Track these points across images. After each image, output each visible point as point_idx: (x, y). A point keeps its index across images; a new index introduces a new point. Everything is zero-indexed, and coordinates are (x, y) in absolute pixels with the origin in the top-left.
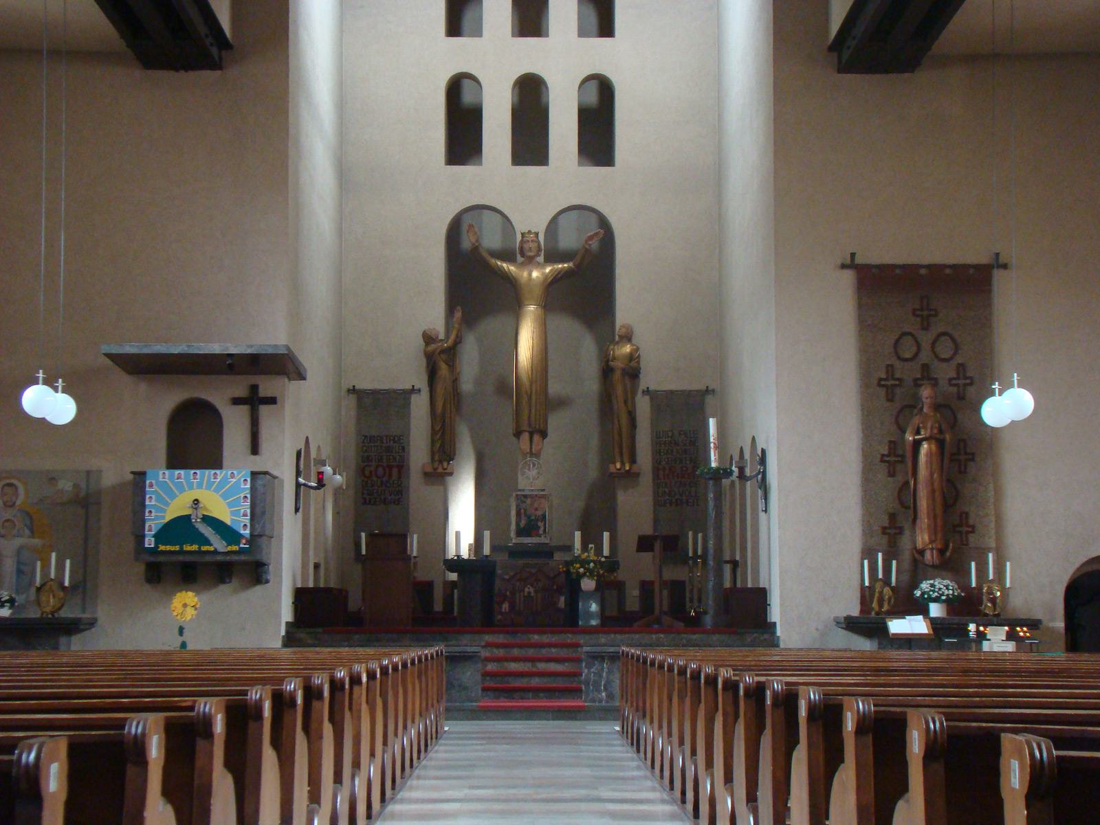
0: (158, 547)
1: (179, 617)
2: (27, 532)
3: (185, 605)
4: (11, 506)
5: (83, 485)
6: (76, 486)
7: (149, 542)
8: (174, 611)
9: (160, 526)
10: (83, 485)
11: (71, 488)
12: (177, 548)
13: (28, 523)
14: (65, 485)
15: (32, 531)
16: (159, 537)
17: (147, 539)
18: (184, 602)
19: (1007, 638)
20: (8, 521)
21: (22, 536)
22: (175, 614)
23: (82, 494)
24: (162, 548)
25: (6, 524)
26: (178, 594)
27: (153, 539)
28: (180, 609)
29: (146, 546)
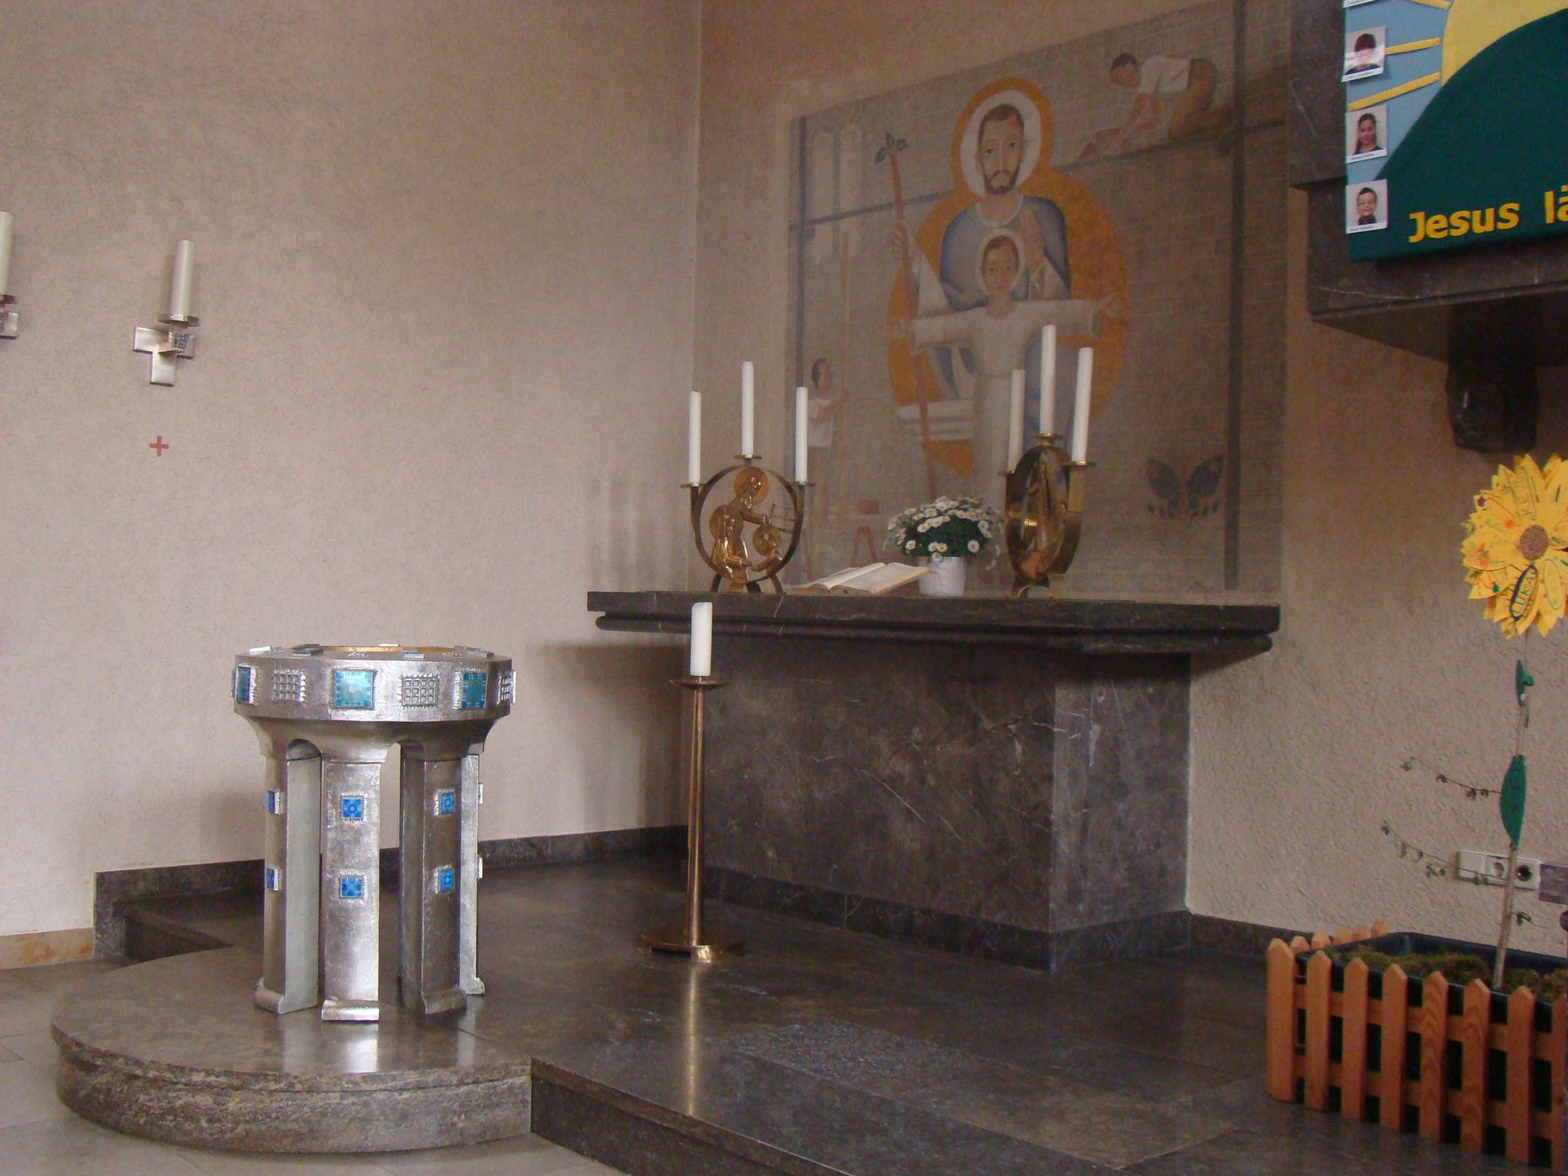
0: (1412, 227)
1: (1500, 613)
2: (1052, 279)
3: (1534, 543)
4: (1004, 190)
5: (1222, 60)
6: (1199, 69)
7: (1365, 205)
8: (1477, 573)
9: (1412, 113)
10: (1222, 60)
11: (1182, 84)
12: (1509, 216)
13: (1054, 242)
14: (1165, 75)
15: (1065, 276)
16: (1410, 175)
17: (1351, 192)
18: (1528, 523)
19: (1261, 950)
20: (995, 244)
21: (1038, 296)
22: (1480, 591)
23: (1222, 95)
24: (1428, 227)
25: (992, 256)
26: (1502, 476)
27: (1381, 188)
28: (1506, 562)
29: (1352, 227)
